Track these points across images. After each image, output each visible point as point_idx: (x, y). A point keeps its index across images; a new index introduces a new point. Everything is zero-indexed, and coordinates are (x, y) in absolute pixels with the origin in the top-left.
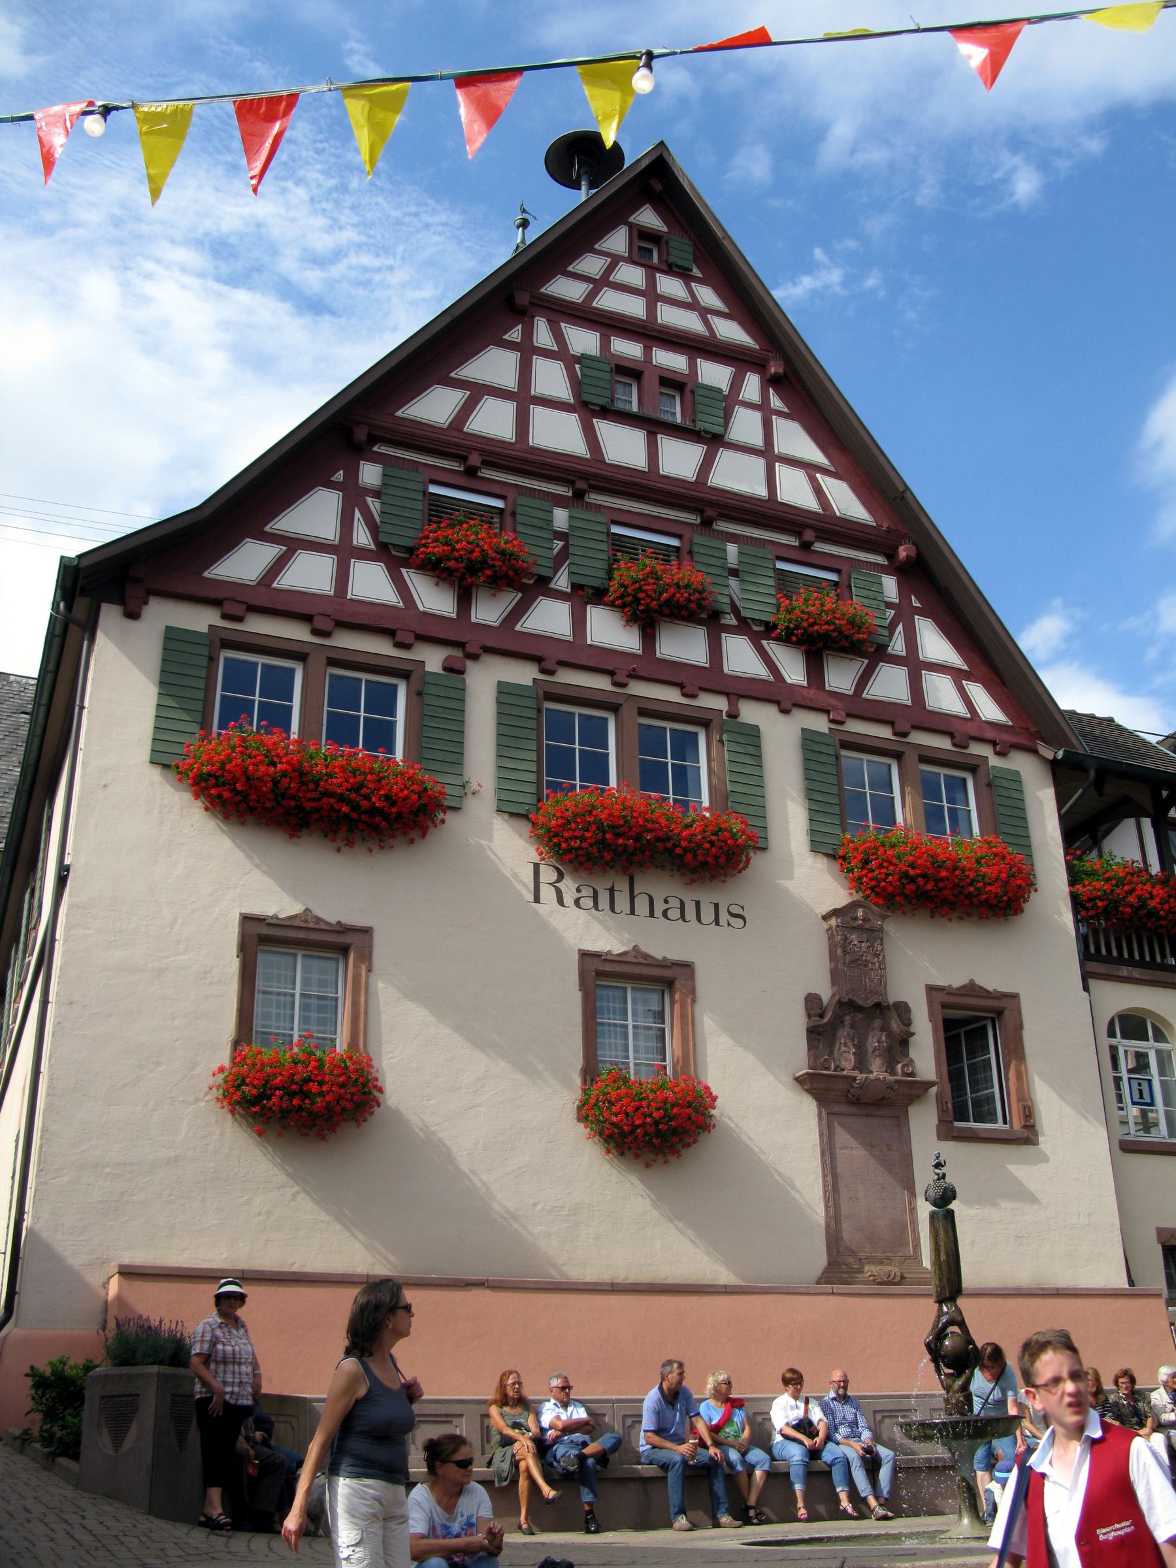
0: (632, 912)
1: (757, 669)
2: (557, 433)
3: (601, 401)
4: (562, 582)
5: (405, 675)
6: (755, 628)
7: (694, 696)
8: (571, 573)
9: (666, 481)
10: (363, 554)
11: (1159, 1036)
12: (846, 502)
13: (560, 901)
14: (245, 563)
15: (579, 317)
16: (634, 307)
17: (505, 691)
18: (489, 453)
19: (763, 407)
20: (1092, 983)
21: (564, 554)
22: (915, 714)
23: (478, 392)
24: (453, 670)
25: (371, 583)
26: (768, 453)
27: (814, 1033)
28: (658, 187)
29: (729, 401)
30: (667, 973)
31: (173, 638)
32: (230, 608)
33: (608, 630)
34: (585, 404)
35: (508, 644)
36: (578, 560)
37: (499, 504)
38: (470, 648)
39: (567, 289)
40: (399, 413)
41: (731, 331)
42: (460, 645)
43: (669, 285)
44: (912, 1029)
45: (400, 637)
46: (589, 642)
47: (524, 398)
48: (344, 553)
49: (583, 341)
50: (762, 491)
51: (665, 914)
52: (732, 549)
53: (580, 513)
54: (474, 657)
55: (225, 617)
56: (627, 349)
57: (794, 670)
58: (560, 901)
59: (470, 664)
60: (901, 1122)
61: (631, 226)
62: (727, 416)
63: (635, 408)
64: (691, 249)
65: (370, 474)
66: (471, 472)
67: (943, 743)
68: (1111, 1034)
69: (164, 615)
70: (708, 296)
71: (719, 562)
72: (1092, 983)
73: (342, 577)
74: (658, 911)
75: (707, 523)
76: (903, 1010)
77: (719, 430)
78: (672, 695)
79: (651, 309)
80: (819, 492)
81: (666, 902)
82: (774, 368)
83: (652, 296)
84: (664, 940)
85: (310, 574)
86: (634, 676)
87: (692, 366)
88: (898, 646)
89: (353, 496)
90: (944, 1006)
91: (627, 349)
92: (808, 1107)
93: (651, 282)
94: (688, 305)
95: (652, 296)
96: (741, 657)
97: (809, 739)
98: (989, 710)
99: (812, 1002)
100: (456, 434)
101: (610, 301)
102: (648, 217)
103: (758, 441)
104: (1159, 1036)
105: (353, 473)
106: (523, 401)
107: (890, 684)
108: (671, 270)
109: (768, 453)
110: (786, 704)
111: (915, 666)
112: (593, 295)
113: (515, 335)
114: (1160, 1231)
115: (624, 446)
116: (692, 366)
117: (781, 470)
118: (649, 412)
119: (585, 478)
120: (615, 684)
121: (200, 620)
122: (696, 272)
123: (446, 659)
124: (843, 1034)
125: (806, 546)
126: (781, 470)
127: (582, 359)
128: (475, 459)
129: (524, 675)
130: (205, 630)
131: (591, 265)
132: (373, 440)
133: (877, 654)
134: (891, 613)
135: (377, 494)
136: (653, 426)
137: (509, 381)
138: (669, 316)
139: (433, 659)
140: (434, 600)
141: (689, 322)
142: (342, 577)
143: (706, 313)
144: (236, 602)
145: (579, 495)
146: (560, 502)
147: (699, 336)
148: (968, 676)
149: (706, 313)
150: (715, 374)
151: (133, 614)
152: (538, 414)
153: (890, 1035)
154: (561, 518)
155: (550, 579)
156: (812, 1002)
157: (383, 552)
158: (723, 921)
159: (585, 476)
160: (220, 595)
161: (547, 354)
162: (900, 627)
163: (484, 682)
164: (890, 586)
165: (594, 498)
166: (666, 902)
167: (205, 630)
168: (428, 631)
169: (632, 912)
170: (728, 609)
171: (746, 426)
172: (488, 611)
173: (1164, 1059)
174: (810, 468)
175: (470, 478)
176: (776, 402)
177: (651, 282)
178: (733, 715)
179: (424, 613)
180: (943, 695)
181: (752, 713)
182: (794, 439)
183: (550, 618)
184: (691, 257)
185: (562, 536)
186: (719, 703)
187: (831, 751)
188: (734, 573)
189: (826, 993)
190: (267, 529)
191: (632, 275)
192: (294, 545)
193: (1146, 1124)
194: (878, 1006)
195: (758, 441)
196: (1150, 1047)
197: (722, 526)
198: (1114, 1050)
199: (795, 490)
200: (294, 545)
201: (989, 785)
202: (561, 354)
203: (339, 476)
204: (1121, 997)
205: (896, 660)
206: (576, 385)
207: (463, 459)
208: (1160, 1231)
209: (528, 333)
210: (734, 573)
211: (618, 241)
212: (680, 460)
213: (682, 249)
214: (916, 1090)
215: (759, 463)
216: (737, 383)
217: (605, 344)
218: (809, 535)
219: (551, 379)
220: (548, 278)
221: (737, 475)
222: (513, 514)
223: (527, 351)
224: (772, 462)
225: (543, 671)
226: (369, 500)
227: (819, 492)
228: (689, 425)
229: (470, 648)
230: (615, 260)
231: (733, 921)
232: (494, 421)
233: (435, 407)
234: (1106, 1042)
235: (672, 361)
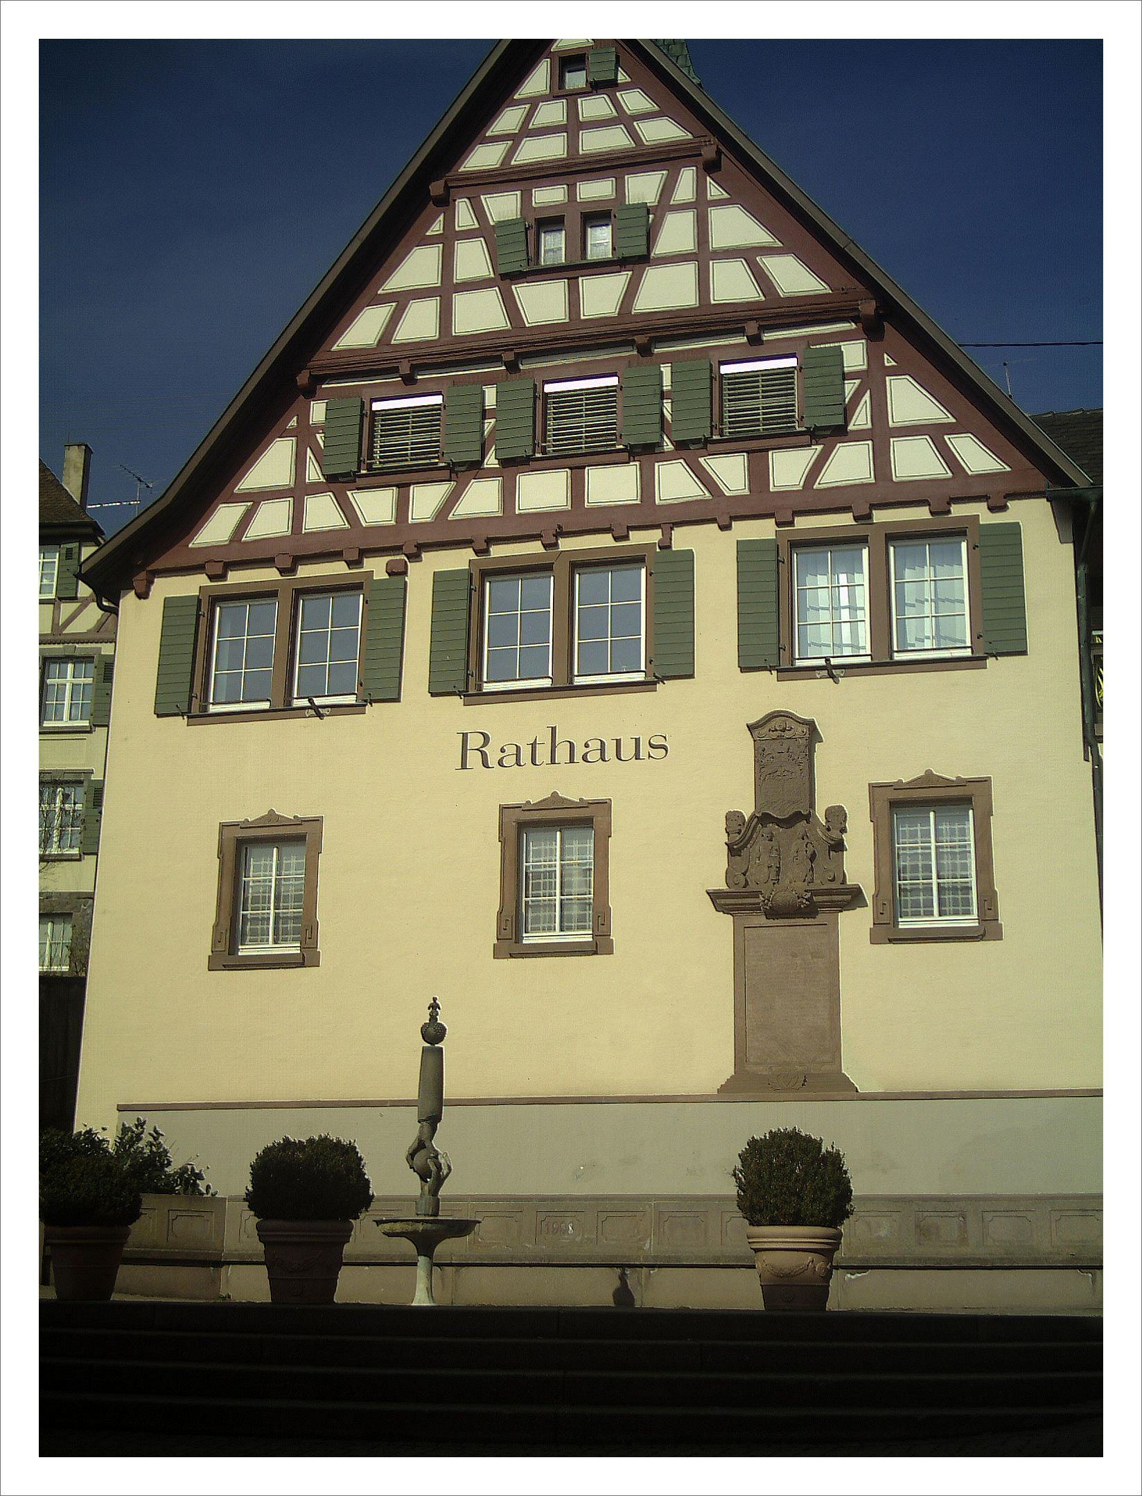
2: (479, 314)
4: (491, 461)
7: (626, 538)
10: (315, 489)
13: (485, 764)
14: (218, 527)
15: (539, 177)
16: (551, 148)
18: (763, 319)
24: (398, 573)
31: (170, 604)
41: (662, 131)
42: (396, 549)
46: (393, 522)
49: (503, 206)
54: (415, 557)
58: (485, 764)
65: (318, 411)
69: (167, 588)
70: (635, 101)
74: (578, 757)
80: (761, 277)
81: (587, 746)
82: (709, 153)
84: (577, 784)
85: (272, 521)
89: (304, 436)
99: (733, 818)
100: (386, 349)
105: (305, 415)
108: (596, 87)
113: (437, 228)
115: (543, 303)
121: (190, 586)
125: (755, 340)
131: (509, 120)
132: (319, 380)
134: (850, 387)
138: (594, 142)
141: (615, 140)
142: (298, 516)
143: (624, 120)
146: (490, 380)
147: (632, 150)
150: (643, 187)
151: (143, 595)
156: (733, 818)
159: (508, 348)
162: (867, 397)
166: (503, 750)
171: (676, 233)
175: (410, 384)
176: (714, 191)
178: (665, 546)
179: (366, 528)
180: (915, 461)
181: (682, 539)
189: (748, 810)
191: (553, 113)
192: (257, 498)
199: (733, 285)
200: (257, 498)
203: (293, 422)
205: (859, 436)
207: (394, 371)
212: (601, 297)
219: (473, 259)
223: (448, 240)
227: (761, 277)
231: (653, 752)
232: (420, 324)
235: (595, 190)
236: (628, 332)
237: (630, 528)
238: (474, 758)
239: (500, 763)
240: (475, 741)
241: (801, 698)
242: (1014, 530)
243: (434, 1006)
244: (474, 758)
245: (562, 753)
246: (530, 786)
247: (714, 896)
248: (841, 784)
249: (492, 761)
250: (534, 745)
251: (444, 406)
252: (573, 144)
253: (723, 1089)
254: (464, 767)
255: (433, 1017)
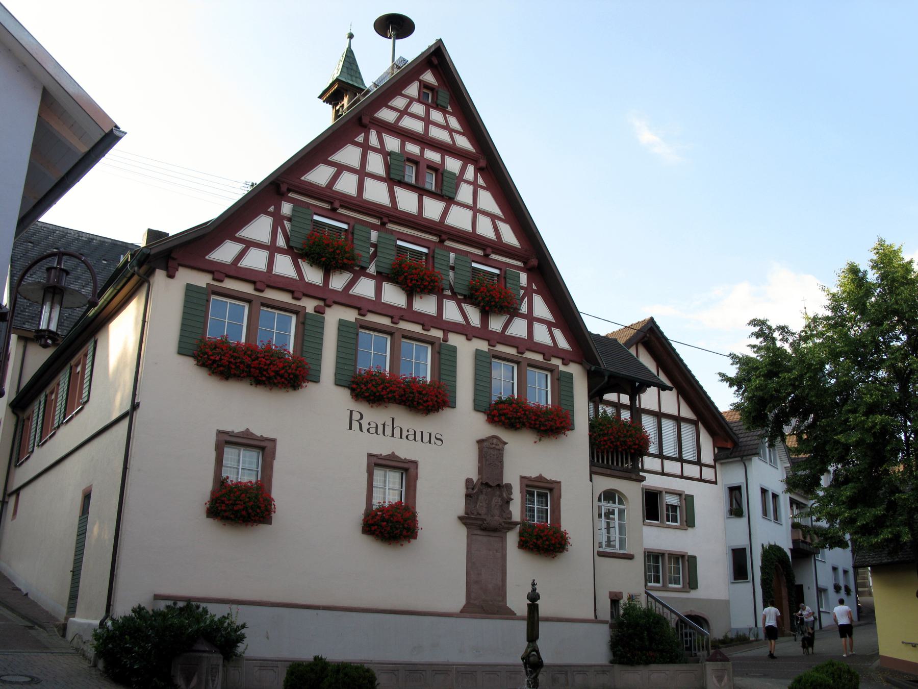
0: (393, 436)
1: (459, 318)
2: (377, 193)
3: (398, 178)
4: (372, 270)
5: (296, 313)
6: (459, 297)
8: (377, 266)
9: (30, 38)
10: (281, 251)
11: (621, 502)
12: (509, 237)
14: (226, 253)
15: (144, 321)
16: (417, 126)
17: (342, 324)
18: (344, 201)
19: (474, 184)
20: (594, 476)
21: (375, 254)
22: (529, 344)
23: (341, 168)
24: (319, 311)
25: (284, 266)
26: (474, 208)
27: (468, 496)
28: (436, 61)
29: (459, 179)
30: (406, 466)
31: (190, 290)
32: (217, 275)
33: (393, 296)
34: (391, 179)
35: (345, 299)
36: (381, 260)
37: (345, 226)
38: (328, 302)
39: (387, 115)
40: (303, 178)
41: (463, 142)
42: (324, 300)
43: (436, 116)
44: (512, 497)
45: (296, 295)
47: (362, 173)
48: (272, 249)
49: (393, 144)
50: (468, 227)
51: (407, 437)
52: (452, 255)
53: (383, 235)
54: (329, 306)
55: (214, 279)
56: (413, 149)
57: (475, 318)
59: (327, 309)
60: (503, 540)
61: (420, 82)
62: (457, 187)
63: (413, 182)
64: (448, 97)
65: (287, 208)
66: (334, 210)
67: (539, 358)
68: (600, 500)
69: (187, 277)
70: (454, 123)
71: (445, 263)
72: (594, 476)
73: (271, 262)
74: (404, 436)
75: (442, 241)
76: (509, 487)
77: (451, 195)
78: (418, 329)
79: (426, 129)
82: (483, 163)
83: (427, 121)
84: (405, 450)
85: (256, 260)
86: (402, 318)
87: (443, 160)
88: (524, 309)
89: (278, 220)
90: (527, 486)
91: (413, 149)
92: (463, 531)
93: (428, 113)
94: (444, 127)
95: (427, 121)
96: (451, 312)
97: (478, 354)
98: (563, 343)
99: (469, 481)
101: (408, 123)
102: (429, 77)
103: (470, 201)
104: (621, 502)
105: (278, 208)
106: (360, 177)
107: (518, 328)
108: (438, 107)
109: (474, 208)
110: (470, 336)
111: (531, 319)
112: (399, 119)
113: (360, 139)
114: (610, 593)
115: (407, 201)
116: (443, 160)
117: (480, 217)
118: (420, 185)
119: (388, 216)
120: (392, 322)
121: (202, 280)
122: (449, 109)
123: (315, 307)
124: (481, 497)
126: (480, 217)
127: (390, 154)
128: (337, 204)
129: (350, 315)
130: (205, 286)
131: (399, 102)
132: (289, 190)
133: (514, 313)
134: (522, 292)
135: (290, 220)
136: (422, 192)
137: (356, 164)
138: (437, 134)
139: (309, 305)
140: (313, 276)
142: (271, 262)
143: (451, 131)
144: (219, 272)
145: (383, 224)
146: (374, 227)
147: (448, 144)
148: (556, 326)
149: (451, 131)
150: (453, 165)
151: (171, 276)
152: (368, 182)
153: (503, 499)
154: (374, 236)
155: (366, 268)
156: (469, 481)
157: (291, 251)
158: (432, 442)
159: (388, 216)
160: (214, 269)
161: (375, 150)
162: (526, 299)
163: (334, 316)
164: (523, 278)
165: (390, 226)
167: (205, 286)
168: (309, 291)
169: (393, 436)
170: (448, 287)
171: (465, 193)
172: (338, 282)
173: (621, 512)
174: (493, 217)
175: (332, 213)
176: (481, 181)
177: (428, 113)
180: (541, 335)
181: (455, 340)
182: (487, 201)
183: (365, 288)
184: (448, 101)
185: (375, 246)
186: (438, 334)
187: (488, 360)
188: (453, 268)
189: (475, 477)
190: (237, 235)
191: (418, 109)
193: (609, 543)
194: (498, 485)
195: (470, 201)
196: (616, 507)
197: (448, 243)
198: (599, 507)
199: (485, 228)
200: (249, 244)
201: (558, 379)
202: (382, 151)
203: (272, 209)
204: (606, 483)
206: (388, 167)
208: (610, 593)
209: (367, 139)
210: (453, 268)
211: (413, 90)
212: (433, 209)
213: (444, 96)
214: (511, 525)
215: (469, 213)
216: (463, 170)
217: (403, 146)
218: (489, 251)
219: (376, 164)
220: (379, 108)
221: (459, 219)
222: (353, 233)
224: (471, 211)
225: (360, 314)
226: (285, 222)
228: (439, 192)
229: (328, 302)
230: (412, 100)
232: (347, 185)
233: (320, 175)
234: (597, 503)
235: (433, 156)
236: (441, 231)
237: (370, 311)
238: (355, 425)
239: (368, 430)
240: (356, 416)
241: (504, 435)
242: (570, 376)
243: (534, 584)
244: (355, 425)
245: (397, 432)
246: (384, 446)
247: (461, 518)
248: (512, 476)
249: (365, 428)
250: (384, 425)
251: (498, 275)
252: (399, 119)
253: (462, 612)
254: (350, 428)
255: (534, 590)
